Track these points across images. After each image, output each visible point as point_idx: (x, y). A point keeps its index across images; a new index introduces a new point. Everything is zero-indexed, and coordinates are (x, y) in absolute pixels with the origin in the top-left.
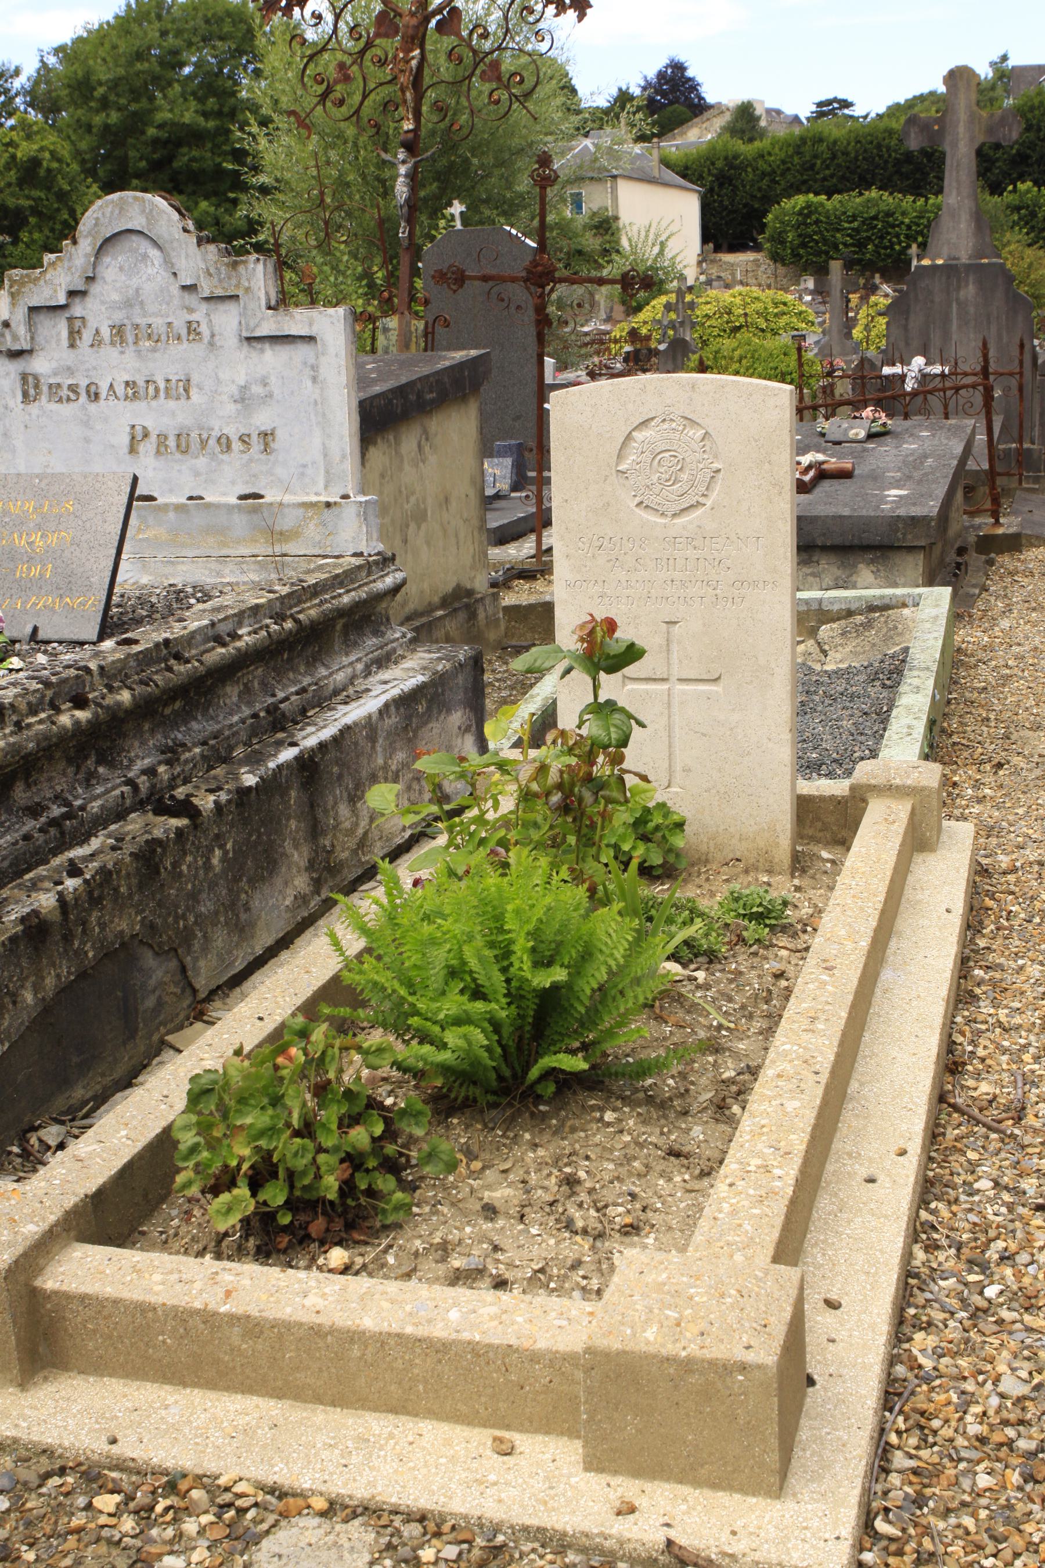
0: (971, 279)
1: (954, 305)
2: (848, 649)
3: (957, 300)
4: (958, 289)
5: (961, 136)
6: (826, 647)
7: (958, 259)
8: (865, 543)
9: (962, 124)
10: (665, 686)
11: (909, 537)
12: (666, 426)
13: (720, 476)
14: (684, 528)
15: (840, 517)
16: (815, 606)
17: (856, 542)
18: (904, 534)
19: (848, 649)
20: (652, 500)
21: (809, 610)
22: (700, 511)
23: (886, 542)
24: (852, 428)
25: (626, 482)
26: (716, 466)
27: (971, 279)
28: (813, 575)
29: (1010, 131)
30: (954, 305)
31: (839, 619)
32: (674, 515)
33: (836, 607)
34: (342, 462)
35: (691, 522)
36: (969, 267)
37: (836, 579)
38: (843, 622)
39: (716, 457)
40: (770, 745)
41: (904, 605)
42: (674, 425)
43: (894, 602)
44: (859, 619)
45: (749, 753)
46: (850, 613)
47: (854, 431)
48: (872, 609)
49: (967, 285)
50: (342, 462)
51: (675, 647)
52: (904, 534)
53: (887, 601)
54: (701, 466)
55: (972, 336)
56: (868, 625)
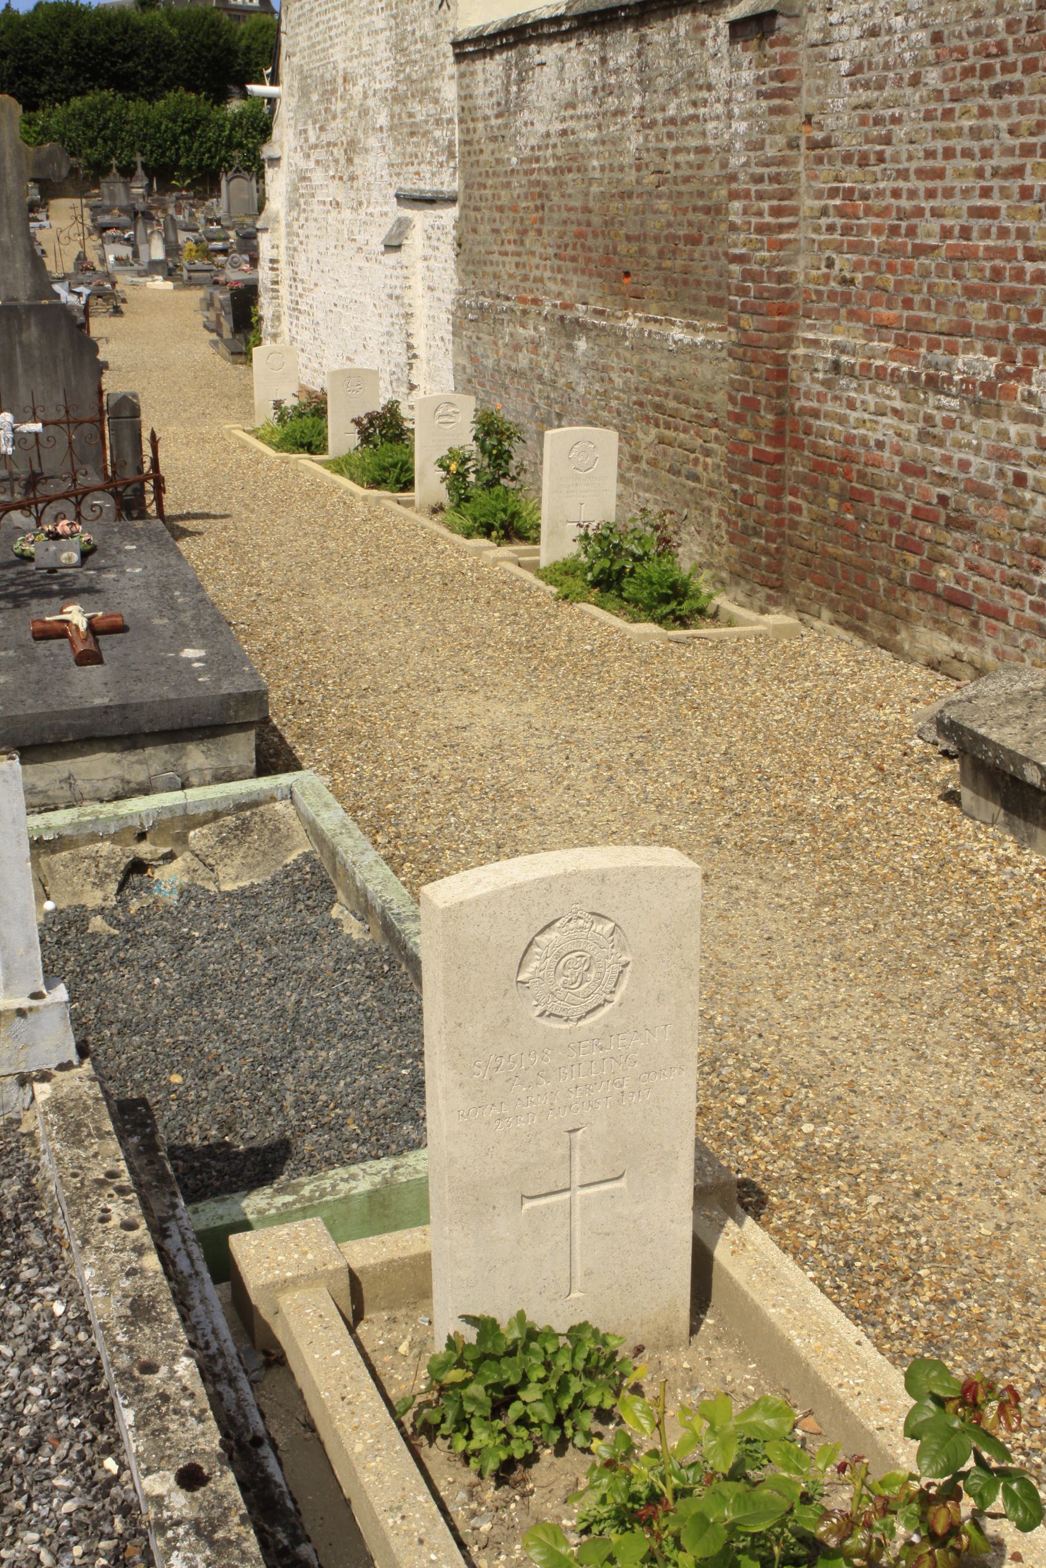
0: (33, 321)
1: (18, 349)
2: (238, 861)
3: (21, 343)
4: (20, 331)
5: (8, 170)
6: (210, 861)
7: (16, 300)
8: (195, 724)
9: (8, 158)
10: (566, 1195)
11: (242, 713)
12: (572, 925)
13: (629, 968)
14: (590, 1030)
15: (169, 701)
16: (179, 813)
17: (186, 724)
18: (236, 712)
19: (238, 861)
20: (555, 1007)
21: (173, 818)
22: (608, 1007)
23: (217, 720)
24: (62, 551)
25: (528, 992)
26: (624, 959)
27: (33, 321)
28: (140, 762)
29: (60, 166)
30: (18, 349)
31: (206, 822)
32: (579, 1019)
33: (202, 810)
34: (27, 952)
35: (597, 1023)
36: (29, 309)
37: (165, 764)
38: (212, 825)
39: (624, 949)
40: (673, 1226)
41: (273, 799)
42: (581, 922)
43: (262, 796)
44: (230, 820)
45: (652, 1240)
46: (216, 815)
47: (65, 555)
48: (240, 807)
49: (29, 327)
50: (27, 952)
51: (577, 1155)
52: (236, 712)
53: (255, 797)
54: (610, 961)
55: (39, 380)
56: (244, 828)
